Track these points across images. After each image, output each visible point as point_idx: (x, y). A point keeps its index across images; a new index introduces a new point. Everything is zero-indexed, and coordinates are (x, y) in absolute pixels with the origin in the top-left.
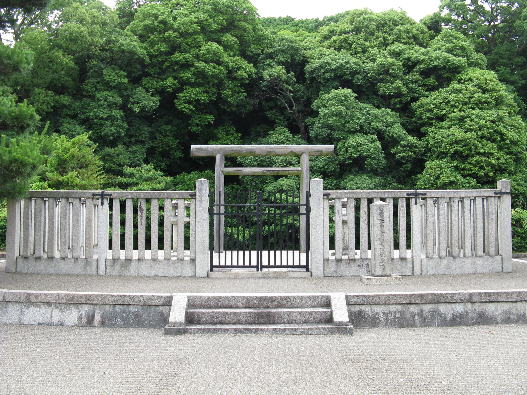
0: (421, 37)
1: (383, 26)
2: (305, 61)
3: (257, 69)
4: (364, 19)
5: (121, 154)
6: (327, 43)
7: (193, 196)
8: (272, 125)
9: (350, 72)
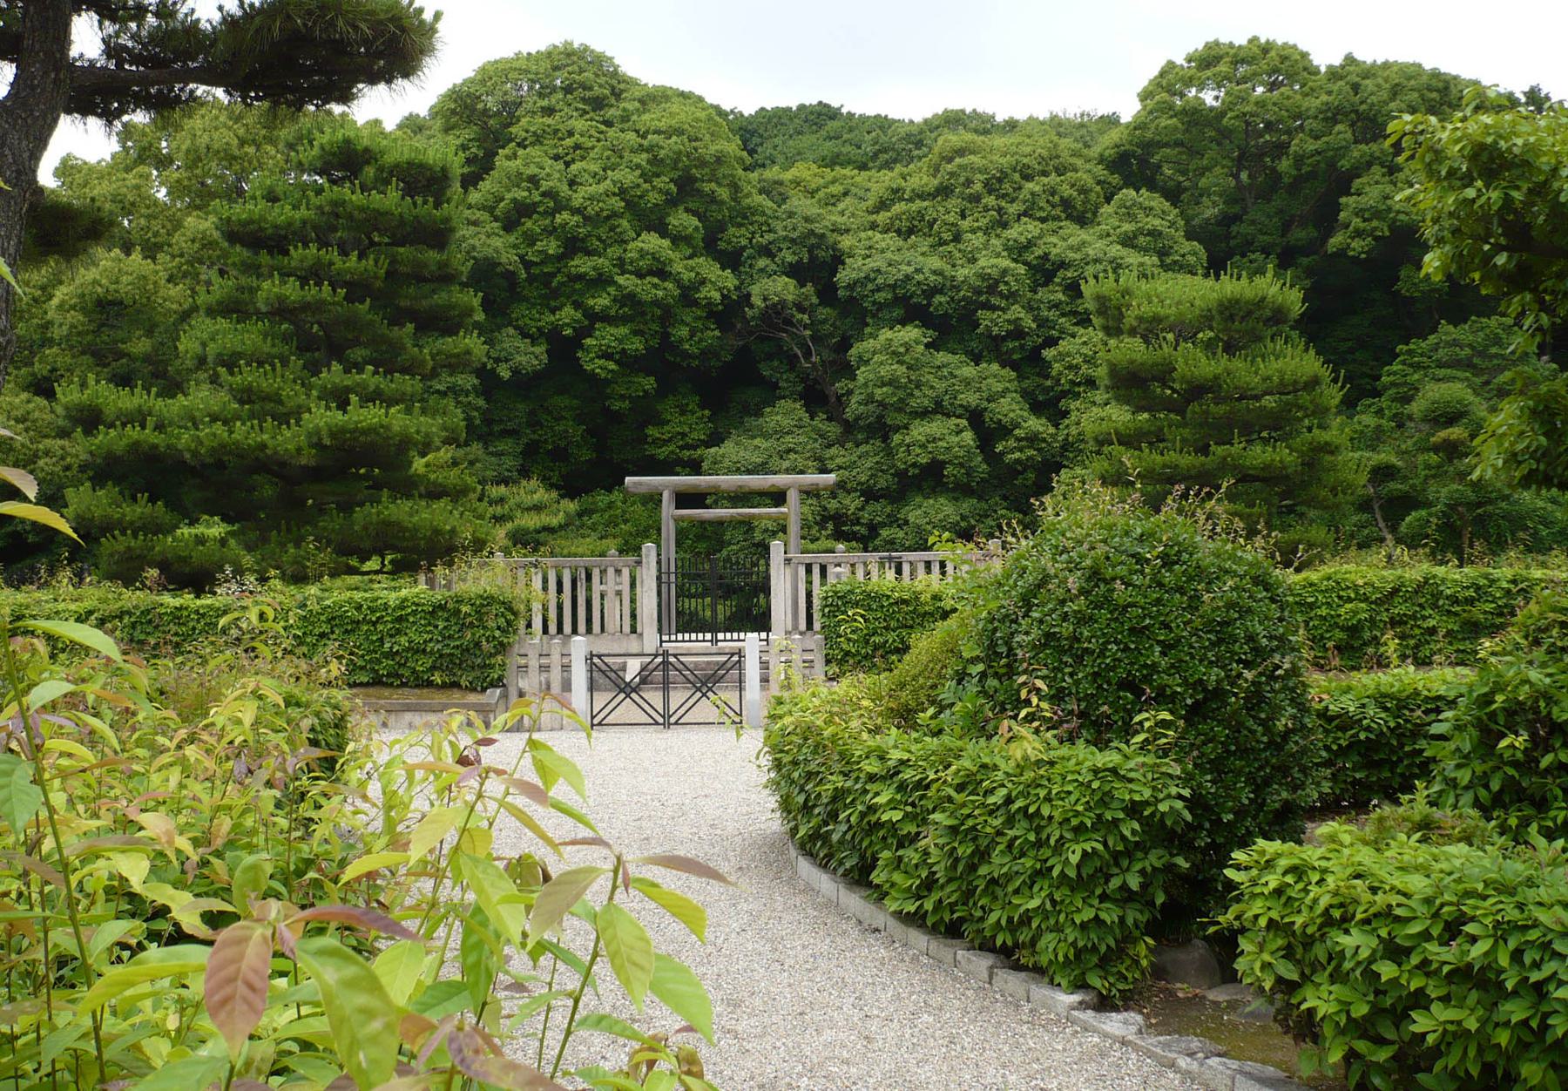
0: (1079, 201)
1: (1000, 180)
2: (838, 260)
3: (738, 277)
4: (959, 166)
5: (477, 460)
6: (882, 218)
7: (639, 563)
8: (771, 392)
9: (924, 291)
